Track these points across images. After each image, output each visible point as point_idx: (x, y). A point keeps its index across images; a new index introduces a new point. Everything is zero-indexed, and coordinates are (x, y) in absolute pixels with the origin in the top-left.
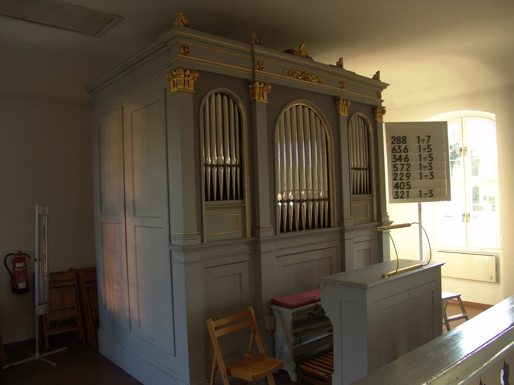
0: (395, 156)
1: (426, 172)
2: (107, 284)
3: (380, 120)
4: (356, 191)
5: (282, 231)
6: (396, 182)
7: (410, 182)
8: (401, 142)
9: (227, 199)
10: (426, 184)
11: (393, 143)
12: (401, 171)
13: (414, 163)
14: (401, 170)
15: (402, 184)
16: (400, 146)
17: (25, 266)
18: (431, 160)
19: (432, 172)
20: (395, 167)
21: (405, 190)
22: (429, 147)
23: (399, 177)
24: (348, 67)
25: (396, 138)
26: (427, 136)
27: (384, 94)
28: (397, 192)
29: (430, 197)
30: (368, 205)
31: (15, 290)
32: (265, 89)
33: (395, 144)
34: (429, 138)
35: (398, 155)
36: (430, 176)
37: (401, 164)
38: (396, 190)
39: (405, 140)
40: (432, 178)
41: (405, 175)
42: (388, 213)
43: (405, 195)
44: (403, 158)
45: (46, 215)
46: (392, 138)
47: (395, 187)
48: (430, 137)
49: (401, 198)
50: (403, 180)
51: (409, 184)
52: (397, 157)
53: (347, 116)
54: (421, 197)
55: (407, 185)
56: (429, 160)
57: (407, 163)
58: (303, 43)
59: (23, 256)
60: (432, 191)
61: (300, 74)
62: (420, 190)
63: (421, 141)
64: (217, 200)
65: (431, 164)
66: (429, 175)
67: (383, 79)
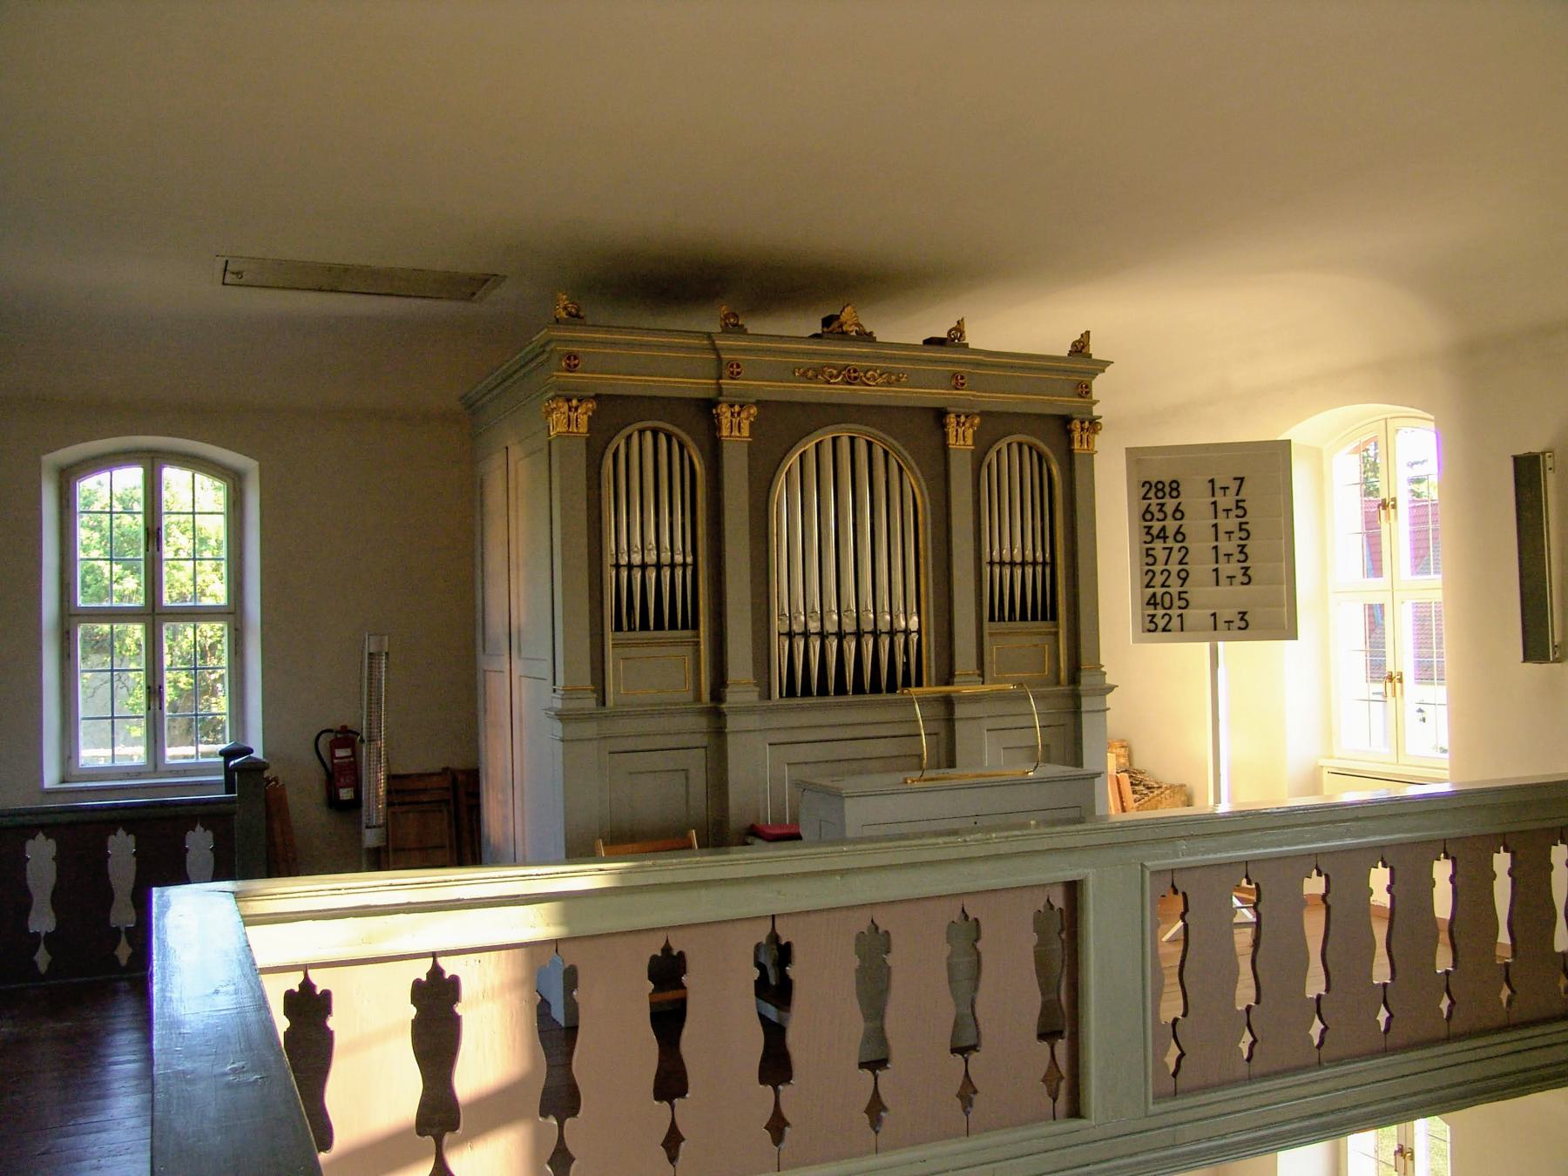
0: (1150, 528)
1: (1228, 568)
2: (491, 792)
3: (1086, 447)
4: (998, 610)
5: (791, 692)
6: (1151, 590)
7: (1186, 592)
8: (1167, 496)
9: (676, 628)
10: (1231, 598)
11: (1144, 498)
12: (1166, 564)
13: (1200, 546)
14: (1164, 562)
15: (1167, 597)
16: (1162, 505)
17: (354, 755)
18: (1244, 537)
19: (1247, 569)
20: (1148, 555)
21: (1175, 612)
22: (1241, 504)
23: (1159, 579)
24: (978, 338)
25: (1153, 485)
26: (1236, 479)
27: (1099, 385)
28: (1153, 616)
29: (1240, 628)
30: (1046, 646)
31: (333, 803)
32: (744, 415)
33: (1150, 499)
34: (1242, 483)
35: (1157, 526)
36: (1240, 578)
37: (1164, 548)
38: (1152, 612)
39: (1177, 489)
40: (1248, 583)
41: (1174, 574)
42: (1103, 666)
43: (1176, 622)
44: (1170, 532)
45: (384, 654)
46: (1143, 486)
47: (1148, 604)
48: (1242, 479)
49: (1164, 630)
50: (1169, 586)
51: (1183, 596)
52: (1155, 532)
53: (973, 447)
54: (1215, 629)
55: (1180, 599)
56: (1241, 539)
57: (1180, 545)
58: (848, 305)
59: (350, 735)
60: (1244, 613)
61: (835, 372)
62: (1213, 612)
63: (1218, 492)
64: (656, 628)
65: (1244, 546)
66: (1239, 573)
67: (1096, 350)
